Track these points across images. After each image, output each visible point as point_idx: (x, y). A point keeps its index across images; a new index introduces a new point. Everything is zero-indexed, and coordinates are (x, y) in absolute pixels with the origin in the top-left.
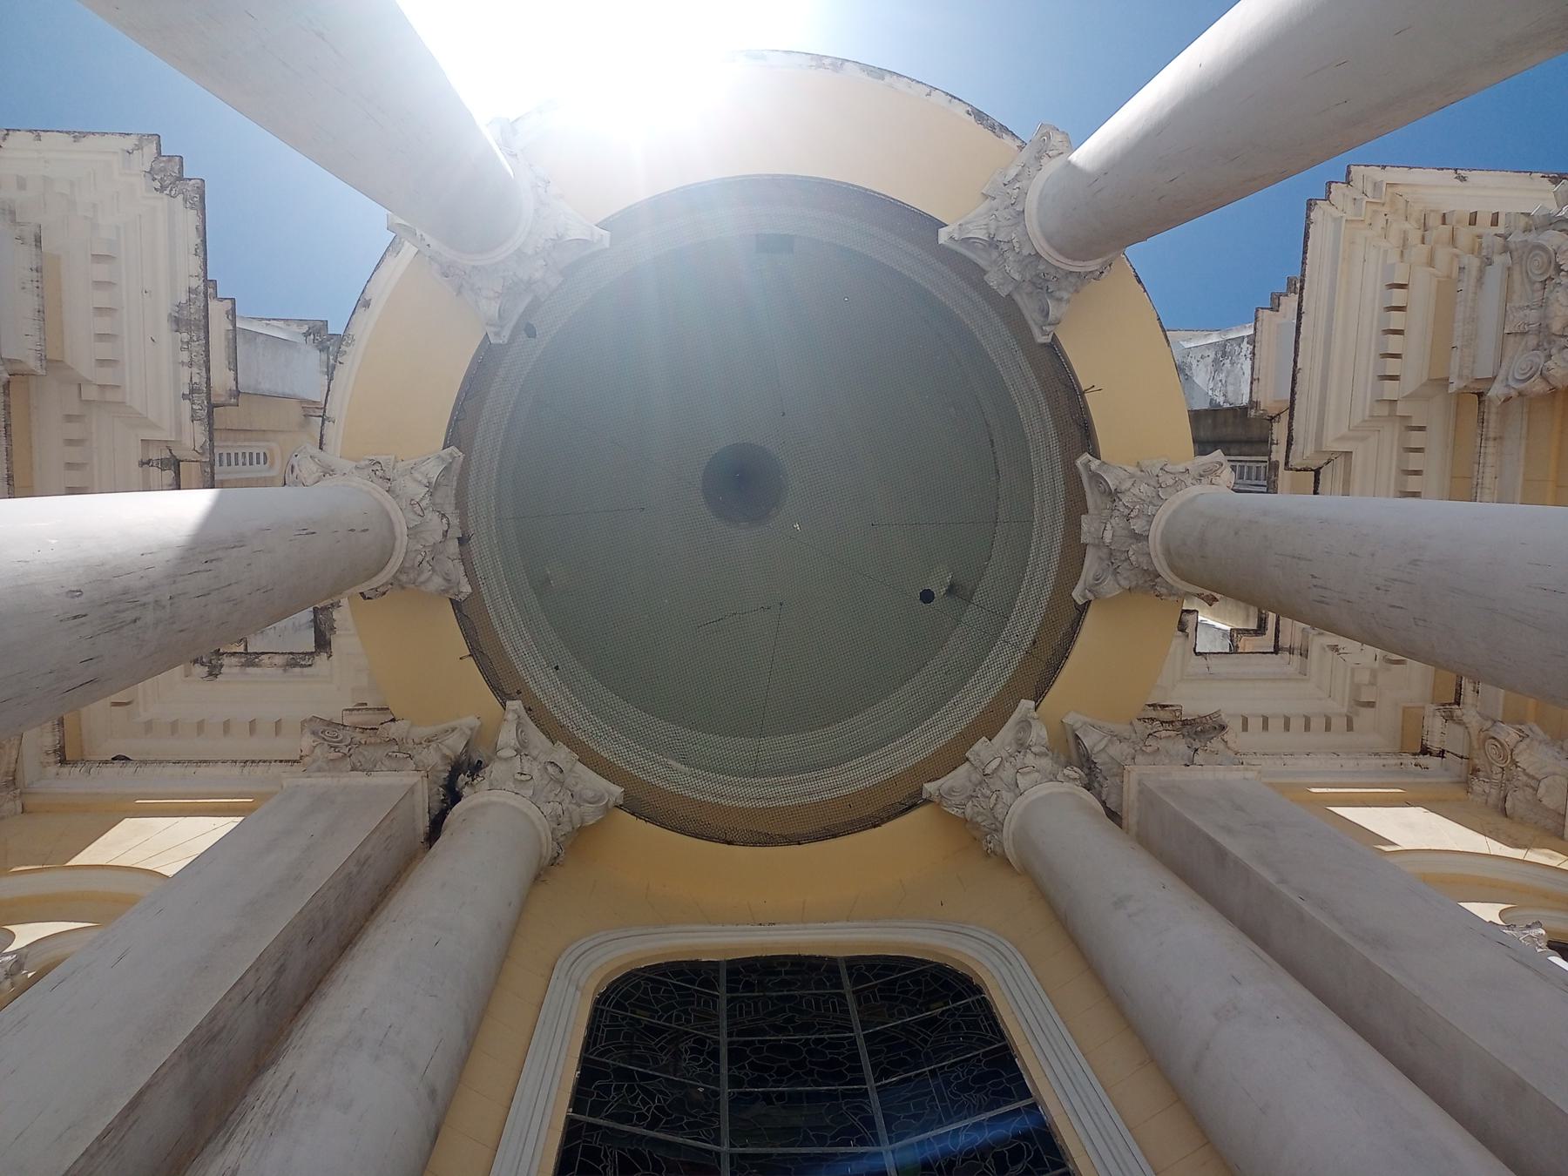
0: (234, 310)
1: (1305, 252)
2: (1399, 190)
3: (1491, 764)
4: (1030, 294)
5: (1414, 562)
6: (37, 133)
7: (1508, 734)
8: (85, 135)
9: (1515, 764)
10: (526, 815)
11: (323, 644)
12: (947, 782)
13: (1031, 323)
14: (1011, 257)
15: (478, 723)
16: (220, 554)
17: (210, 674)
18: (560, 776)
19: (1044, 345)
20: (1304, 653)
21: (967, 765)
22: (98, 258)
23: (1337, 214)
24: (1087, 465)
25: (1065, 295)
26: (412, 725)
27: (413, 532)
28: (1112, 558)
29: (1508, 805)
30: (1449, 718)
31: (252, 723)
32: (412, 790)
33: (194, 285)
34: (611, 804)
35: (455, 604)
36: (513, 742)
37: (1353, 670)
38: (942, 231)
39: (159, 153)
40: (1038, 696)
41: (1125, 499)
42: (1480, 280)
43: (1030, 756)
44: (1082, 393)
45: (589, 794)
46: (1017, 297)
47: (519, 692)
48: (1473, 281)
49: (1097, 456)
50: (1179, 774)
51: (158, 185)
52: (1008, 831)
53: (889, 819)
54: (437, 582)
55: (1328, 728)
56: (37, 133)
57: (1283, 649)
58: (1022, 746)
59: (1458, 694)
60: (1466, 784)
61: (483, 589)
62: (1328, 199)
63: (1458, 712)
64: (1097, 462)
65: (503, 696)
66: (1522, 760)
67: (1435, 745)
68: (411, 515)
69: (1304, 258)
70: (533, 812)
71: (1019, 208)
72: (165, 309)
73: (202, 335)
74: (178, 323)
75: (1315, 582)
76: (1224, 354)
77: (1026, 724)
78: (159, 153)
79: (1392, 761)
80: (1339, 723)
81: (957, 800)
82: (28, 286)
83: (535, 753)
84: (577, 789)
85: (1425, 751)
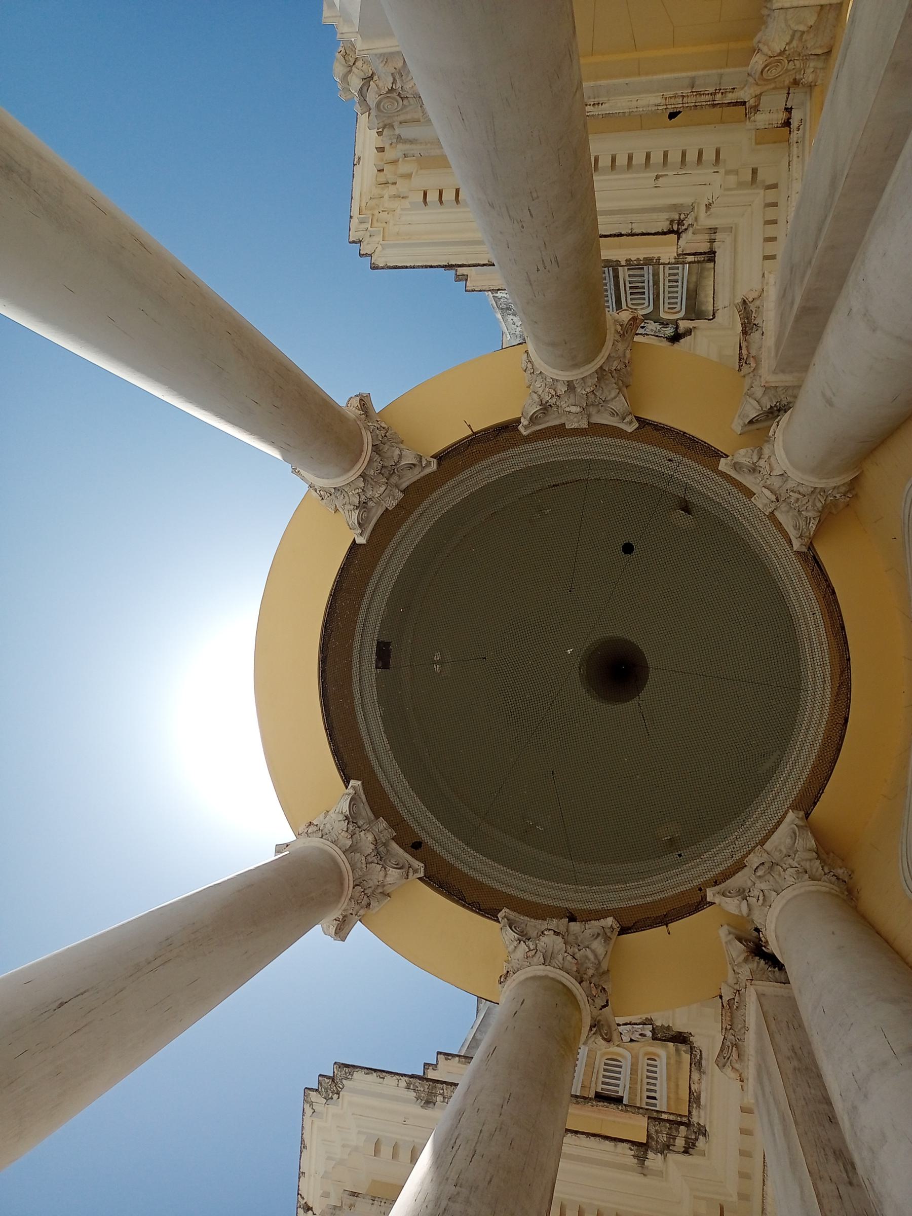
0: (445, 1054)
1: (406, 267)
2: (363, 205)
3: (787, 71)
4: (400, 477)
5: (492, 205)
6: (301, 1174)
7: (758, 61)
8: (302, 1141)
9: (782, 53)
10: (788, 901)
11: (681, 1038)
12: (792, 534)
13: (422, 474)
14: (369, 493)
15: (726, 927)
16: (456, 1134)
17: (704, 1135)
18: (766, 865)
19: (439, 464)
20: (714, 230)
21: (776, 513)
22: (377, 1152)
23: (380, 248)
24: (526, 427)
25: (397, 452)
26: (726, 982)
27: (547, 960)
28: (591, 404)
29: (819, 51)
30: (756, 109)
31: (743, 1110)
32: (760, 996)
33: (405, 1084)
34: (801, 823)
35: (624, 931)
36: (736, 901)
37: (729, 189)
38: (358, 542)
39: (317, 1090)
40: (718, 455)
41: (547, 398)
42: (411, 142)
43: (762, 463)
44: (475, 433)
45: (789, 841)
46: (404, 486)
47: (700, 889)
48: (413, 146)
49: (518, 421)
50: (770, 341)
51: (335, 1096)
52: (821, 484)
53: (827, 580)
54: (598, 946)
55: (775, 205)
56: (301, 1174)
57: (711, 248)
58: (754, 469)
59: (736, 104)
60: (811, 87)
61: (612, 906)
62: (371, 255)
63: (752, 102)
64: (522, 420)
65: (701, 904)
66: (778, 47)
67: (781, 116)
68: (535, 959)
69: (411, 267)
70: (787, 894)
71: (333, 491)
72: (416, 1109)
73: (439, 1085)
74: (429, 1103)
75: (541, 268)
76: (508, 309)
77: (736, 466)
78: (317, 1090)
79: (795, 150)
80: (771, 196)
81: (802, 523)
82: (383, 1210)
83: (749, 883)
84: (785, 851)
85: (787, 123)
